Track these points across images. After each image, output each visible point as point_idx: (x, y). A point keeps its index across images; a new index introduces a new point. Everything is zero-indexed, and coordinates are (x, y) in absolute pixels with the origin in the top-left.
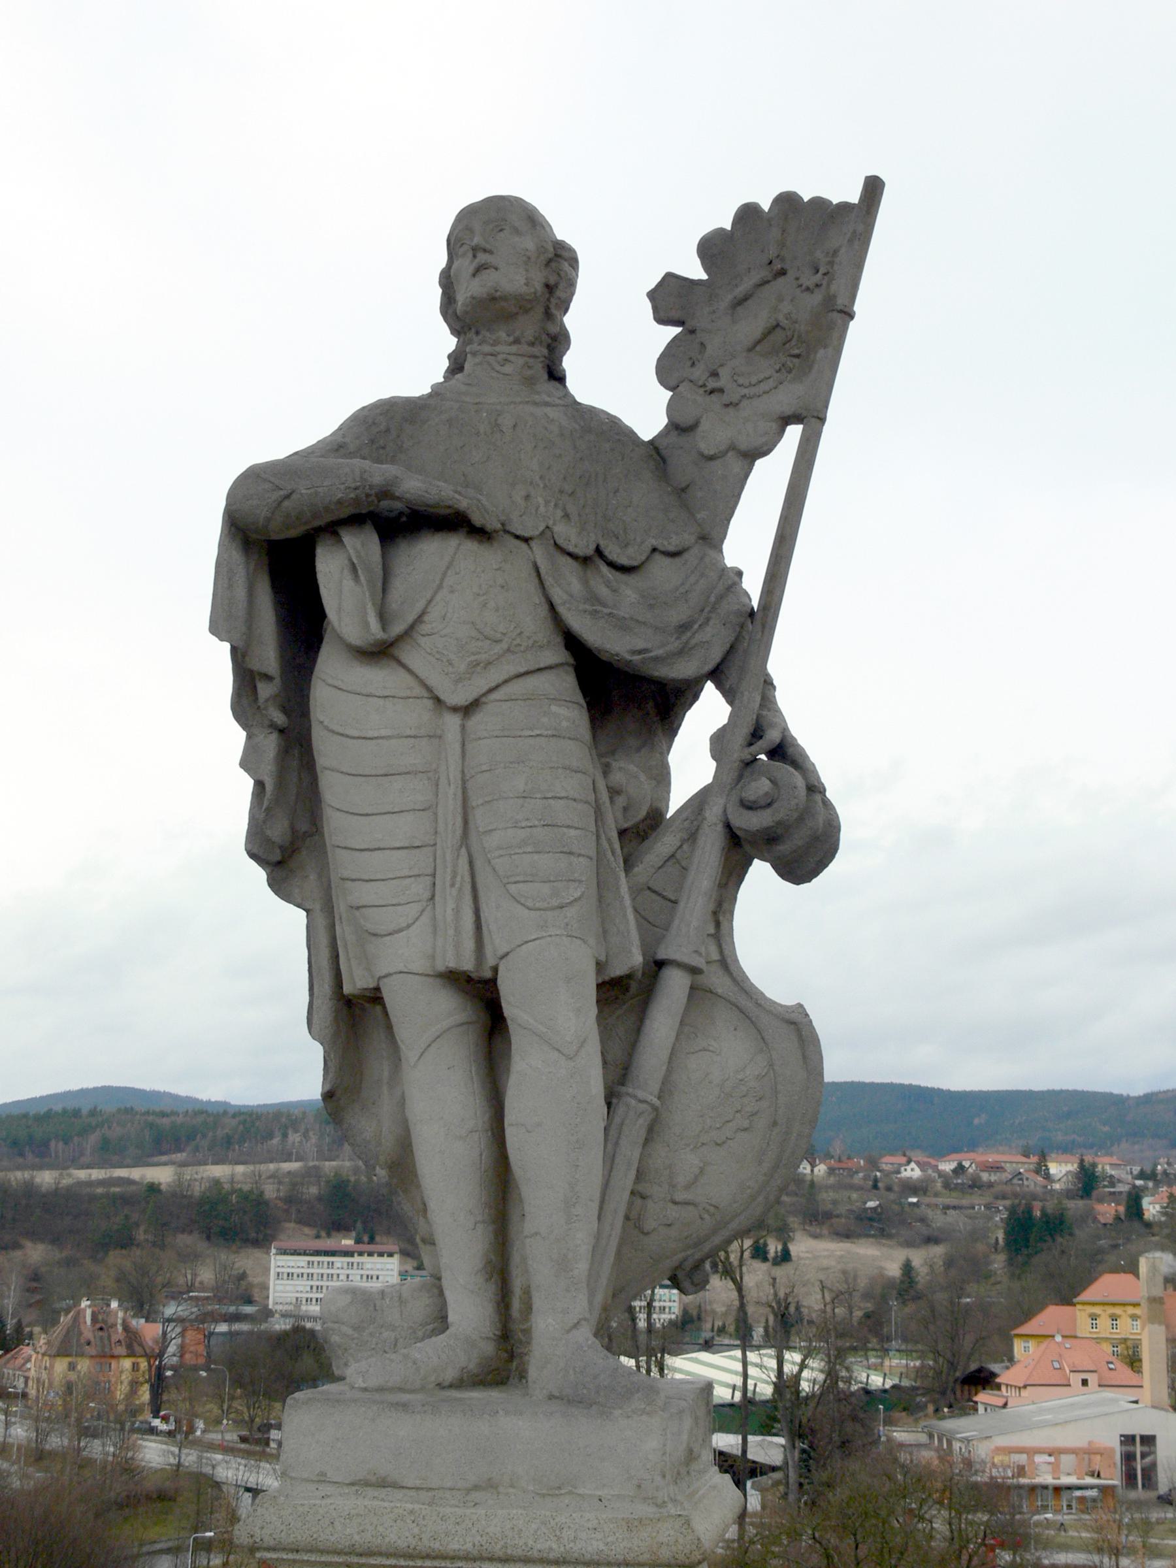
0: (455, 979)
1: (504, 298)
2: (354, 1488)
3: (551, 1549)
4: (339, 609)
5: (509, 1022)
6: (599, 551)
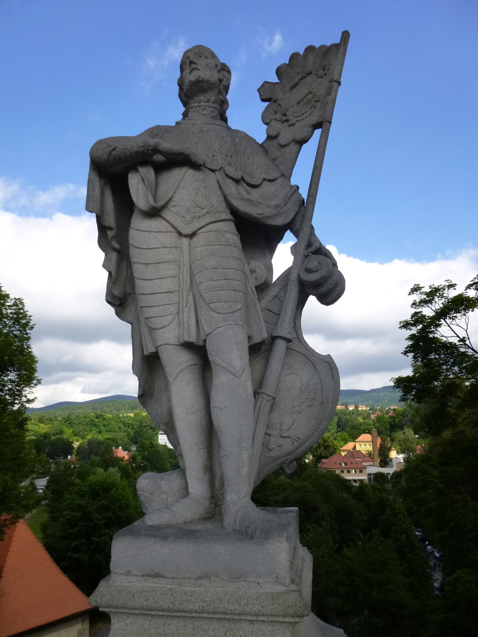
0: (187, 346)
1: (203, 81)
2: (144, 578)
3: (236, 609)
4: (137, 198)
5: (211, 363)
6: (242, 179)
